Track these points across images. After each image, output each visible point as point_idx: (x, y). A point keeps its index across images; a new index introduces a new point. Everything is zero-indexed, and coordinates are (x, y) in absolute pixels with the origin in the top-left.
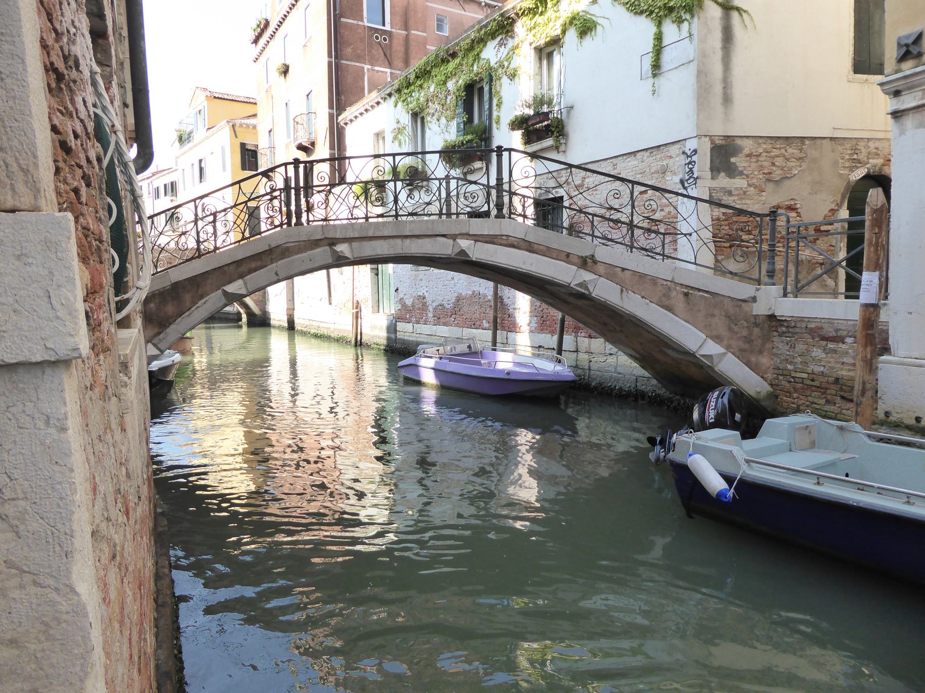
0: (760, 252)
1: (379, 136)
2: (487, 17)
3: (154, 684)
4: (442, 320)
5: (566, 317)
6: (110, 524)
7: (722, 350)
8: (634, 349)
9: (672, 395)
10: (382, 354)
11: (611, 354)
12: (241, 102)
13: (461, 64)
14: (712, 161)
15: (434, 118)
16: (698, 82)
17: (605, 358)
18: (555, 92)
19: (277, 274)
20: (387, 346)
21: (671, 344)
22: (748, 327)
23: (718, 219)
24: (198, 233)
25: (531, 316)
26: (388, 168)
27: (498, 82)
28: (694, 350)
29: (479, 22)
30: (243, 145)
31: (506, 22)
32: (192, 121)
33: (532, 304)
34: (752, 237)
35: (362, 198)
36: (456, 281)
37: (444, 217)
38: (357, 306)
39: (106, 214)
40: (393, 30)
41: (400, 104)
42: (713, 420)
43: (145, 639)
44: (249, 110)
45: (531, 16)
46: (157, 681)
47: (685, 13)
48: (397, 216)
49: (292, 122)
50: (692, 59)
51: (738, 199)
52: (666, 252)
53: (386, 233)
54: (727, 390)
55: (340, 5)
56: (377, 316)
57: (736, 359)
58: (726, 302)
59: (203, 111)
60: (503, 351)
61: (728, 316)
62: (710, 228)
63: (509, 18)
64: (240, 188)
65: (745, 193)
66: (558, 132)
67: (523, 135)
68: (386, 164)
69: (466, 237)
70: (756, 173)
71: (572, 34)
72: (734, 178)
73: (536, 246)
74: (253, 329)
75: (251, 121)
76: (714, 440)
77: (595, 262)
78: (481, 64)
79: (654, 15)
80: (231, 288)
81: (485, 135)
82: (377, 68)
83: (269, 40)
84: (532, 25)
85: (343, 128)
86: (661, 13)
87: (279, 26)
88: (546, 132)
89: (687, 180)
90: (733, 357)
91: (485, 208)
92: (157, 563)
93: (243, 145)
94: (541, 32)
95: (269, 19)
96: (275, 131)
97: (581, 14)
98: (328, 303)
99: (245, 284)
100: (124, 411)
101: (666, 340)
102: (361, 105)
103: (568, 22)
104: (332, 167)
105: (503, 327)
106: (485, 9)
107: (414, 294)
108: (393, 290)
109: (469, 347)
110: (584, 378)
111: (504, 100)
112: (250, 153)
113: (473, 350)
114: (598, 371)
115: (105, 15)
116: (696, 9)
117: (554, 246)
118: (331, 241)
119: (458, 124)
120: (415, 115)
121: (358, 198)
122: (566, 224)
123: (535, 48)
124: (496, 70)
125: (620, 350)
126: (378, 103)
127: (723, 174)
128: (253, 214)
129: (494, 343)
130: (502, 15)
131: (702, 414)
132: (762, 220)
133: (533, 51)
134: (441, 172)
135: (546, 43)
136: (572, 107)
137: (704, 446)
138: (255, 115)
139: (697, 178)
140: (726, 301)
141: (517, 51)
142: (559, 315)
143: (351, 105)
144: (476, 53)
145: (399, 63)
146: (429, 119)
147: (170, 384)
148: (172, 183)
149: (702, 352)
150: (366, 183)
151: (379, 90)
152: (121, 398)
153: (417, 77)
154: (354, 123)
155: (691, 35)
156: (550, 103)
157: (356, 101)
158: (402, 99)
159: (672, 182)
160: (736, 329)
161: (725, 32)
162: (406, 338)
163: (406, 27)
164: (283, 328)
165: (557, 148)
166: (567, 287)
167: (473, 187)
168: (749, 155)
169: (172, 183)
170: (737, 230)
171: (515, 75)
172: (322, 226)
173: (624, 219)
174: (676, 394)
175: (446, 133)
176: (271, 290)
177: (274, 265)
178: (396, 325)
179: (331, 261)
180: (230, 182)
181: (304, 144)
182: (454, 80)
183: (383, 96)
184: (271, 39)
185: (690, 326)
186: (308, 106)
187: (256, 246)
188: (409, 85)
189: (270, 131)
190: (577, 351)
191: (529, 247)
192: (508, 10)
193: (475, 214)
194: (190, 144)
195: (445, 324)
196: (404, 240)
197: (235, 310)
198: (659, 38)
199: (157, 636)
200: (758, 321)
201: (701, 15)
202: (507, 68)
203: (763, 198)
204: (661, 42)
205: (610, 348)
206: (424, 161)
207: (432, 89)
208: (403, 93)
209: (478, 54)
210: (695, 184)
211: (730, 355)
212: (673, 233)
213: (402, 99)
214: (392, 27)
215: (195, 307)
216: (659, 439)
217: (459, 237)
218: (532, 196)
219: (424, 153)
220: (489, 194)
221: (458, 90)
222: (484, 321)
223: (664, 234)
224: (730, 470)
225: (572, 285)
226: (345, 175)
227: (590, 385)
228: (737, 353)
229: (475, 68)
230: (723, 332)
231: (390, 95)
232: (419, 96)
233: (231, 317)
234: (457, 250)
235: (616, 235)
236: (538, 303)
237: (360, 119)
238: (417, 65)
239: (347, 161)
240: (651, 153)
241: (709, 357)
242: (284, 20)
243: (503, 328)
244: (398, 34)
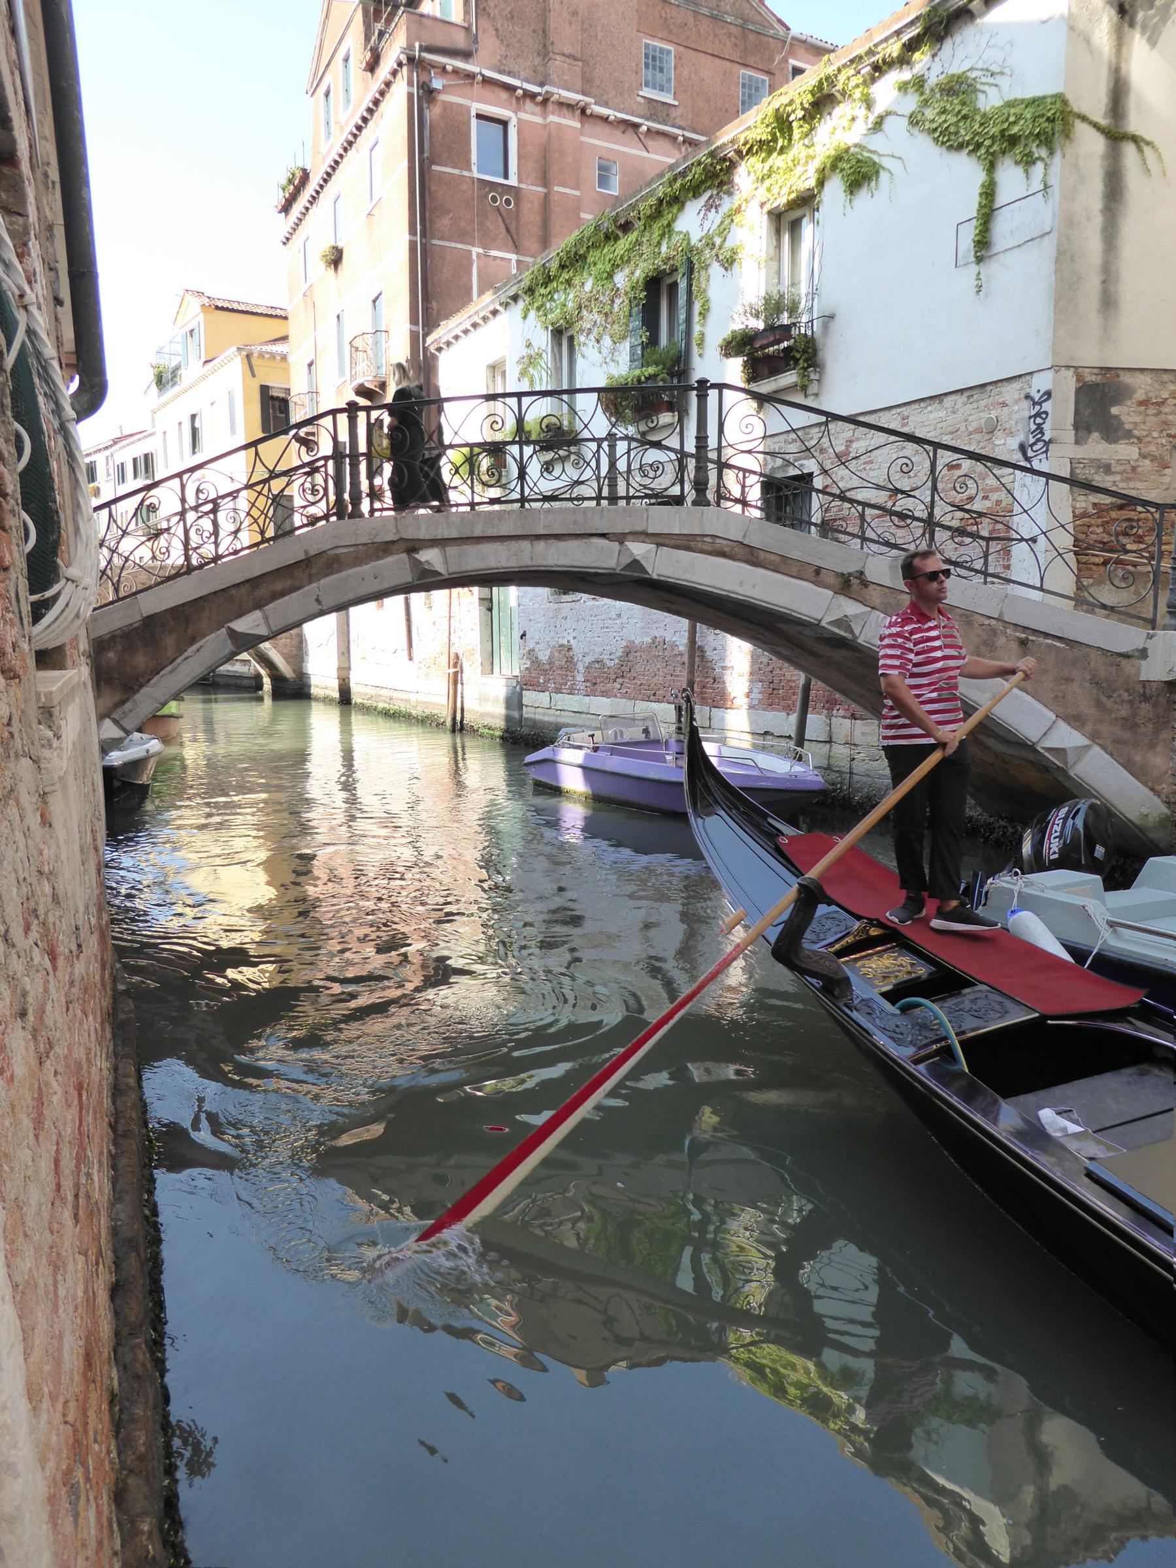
0: (1156, 572)
1: (496, 369)
2: (685, 158)
4: (600, 687)
7: (1084, 741)
9: (992, 819)
10: (498, 747)
13: (638, 243)
14: (1077, 412)
15: (592, 337)
16: (1057, 271)
18: (804, 289)
19: (318, 601)
20: (506, 731)
21: (993, 728)
22: (1130, 702)
23: (1084, 515)
25: (751, 681)
27: (703, 273)
28: (1034, 740)
29: (672, 167)
30: (264, 389)
31: (718, 167)
32: (179, 348)
33: (754, 659)
34: (1142, 546)
35: (464, 470)
36: (624, 620)
37: (604, 503)
38: (456, 662)
39: (13, 450)
40: (522, 186)
41: (532, 314)
42: (1056, 856)
43: (89, 1175)
44: (274, 328)
45: (763, 155)
47: (1038, 146)
48: (523, 500)
49: (347, 348)
50: (1048, 230)
51: (1122, 481)
52: (991, 570)
53: (504, 531)
54: (1083, 805)
55: (431, 142)
56: (489, 679)
57: (1108, 757)
58: (1092, 656)
59: (196, 331)
61: (1095, 682)
62: (1070, 527)
63: (724, 159)
64: (257, 454)
65: (1134, 469)
66: (806, 360)
68: (506, 411)
69: (642, 538)
70: (1155, 434)
71: (835, 187)
72: (1115, 441)
73: (762, 555)
74: (282, 703)
76: (1056, 888)
77: (865, 584)
78: (674, 241)
79: (983, 151)
80: (242, 625)
81: (679, 365)
82: (493, 253)
83: (308, 205)
84: (765, 171)
85: (434, 357)
86: (995, 147)
88: (786, 360)
89: (1032, 446)
90: (1103, 752)
91: (676, 491)
92: (116, 1069)
93: (264, 389)
95: (308, 167)
96: (320, 365)
97: (852, 150)
98: (407, 657)
99: (266, 618)
100: (47, 790)
103: (828, 165)
105: (703, 698)
106: (683, 149)
107: (553, 643)
108: (517, 634)
109: (646, 731)
111: (714, 305)
112: (277, 404)
113: (652, 736)
117: (795, 554)
118: (409, 545)
121: (457, 472)
123: (770, 213)
124: (700, 252)
126: (495, 313)
127: (1095, 435)
128: (281, 502)
130: (712, 154)
132: (1162, 516)
133: (765, 217)
136: (832, 317)
138: (284, 338)
139: (1050, 441)
140: (1093, 655)
141: (737, 218)
142: (800, 678)
143: (447, 317)
144: (666, 223)
145: (531, 243)
146: (582, 339)
147: (144, 790)
148: (146, 456)
149: (1048, 743)
150: (471, 446)
151: (497, 290)
152: (42, 766)
153: (562, 267)
154: (453, 348)
156: (793, 309)
157: (458, 311)
158: (536, 305)
159: (1006, 447)
160: (1109, 704)
161: (1110, 180)
162: (538, 717)
163: (545, 180)
165: (804, 388)
166: (814, 626)
167: (653, 455)
168: (1144, 403)
170: (1117, 534)
173: (920, 512)
174: (1000, 817)
175: (612, 364)
176: (309, 628)
177: (314, 585)
178: (521, 695)
179: (409, 579)
181: (366, 385)
182: (627, 271)
183: (503, 299)
186: (376, 319)
187: (287, 553)
188: (548, 280)
189: (310, 365)
190: (830, 741)
191: (751, 556)
192: (724, 145)
194: (176, 389)
195: (605, 694)
196: (535, 543)
197: (252, 671)
198: (989, 192)
199: (114, 1182)
200: (1148, 692)
202: (720, 248)
203: (1166, 480)
204: (992, 201)
206: (573, 411)
207: (588, 287)
208: (537, 294)
209: (669, 225)
210: (1046, 452)
211: (1096, 749)
212: (1005, 539)
213: (536, 305)
214: (520, 181)
215: (182, 658)
217: (630, 537)
218: (758, 469)
219: (572, 392)
220: (682, 468)
221: (633, 288)
224: (1081, 939)
225: (823, 623)
228: (1110, 748)
229: (664, 248)
230: (1086, 707)
231: (515, 298)
232: (566, 299)
233: (246, 682)
234: (626, 561)
236: (766, 656)
237: (464, 341)
238: (563, 245)
240: (969, 397)
241: (1060, 752)
243: (704, 701)
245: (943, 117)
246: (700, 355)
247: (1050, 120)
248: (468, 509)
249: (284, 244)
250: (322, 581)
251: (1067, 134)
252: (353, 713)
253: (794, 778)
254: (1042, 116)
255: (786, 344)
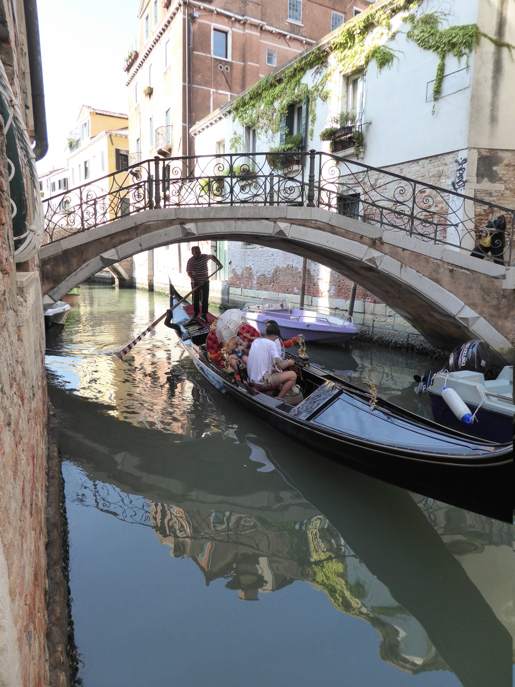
1: (220, 144)
2: (307, 50)
3: (45, 530)
4: (263, 286)
5: (358, 286)
6: (5, 396)
7: (477, 315)
8: (408, 312)
9: (434, 349)
11: (390, 316)
12: (117, 117)
13: (285, 88)
14: (478, 169)
15: (263, 130)
17: (386, 319)
18: (358, 110)
19: (140, 245)
20: (222, 305)
21: (437, 308)
22: (497, 298)
23: (480, 215)
24: (82, 213)
25: (330, 285)
26: (227, 168)
27: (313, 102)
28: (455, 314)
29: (300, 54)
30: (117, 151)
31: (321, 55)
32: (79, 131)
33: (332, 275)
35: (206, 188)
36: (275, 257)
37: (268, 204)
39: (7, 171)
40: (234, 62)
41: (237, 119)
42: (464, 365)
43: (37, 495)
45: (342, 49)
46: (47, 528)
47: (465, 48)
48: (232, 202)
49: (154, 133)
50: (468, 86)
54: (477, 343)
55: (193, 41)
58: (482, 277)
59: (87, 124)
60: (308, 310)
61: (483, 289)
63: (324, 51)
64: (114, 179)
65: (502, 195)
66: (358, 143)
67: (331, 144)
69: (284, 220)
71: (373, 65)
72: (495, 182)
75: (124, 132)
76: (463, 378)
77: (382, 243)
78: (301, 88)
79: (440, 50)
80: (108, 255)
81: (302, 144)
82: (220, 92)
84: (342, 57)
85: (193, 138)
87: (146, 57)
88: (350, 143)
90: (484, 320)
91: (300, 200)
92: (49, 449)
93: (117, 151)
94: (349, 62)
95: (138, 51)
96: (142, 140)
97: (381, 48)
99: (117, 252)
100: (20, 324)
101: (433, 305)
102: (207, 120)
103: (370, 55)
104: (184, 163)
105: (309, 292)
106: (305, 46)
110: (368, 334)
111: (318, 117)
112: (123, 157)
113: (285, 308)
114: (380, 328)
115: (6, 22)
116: (474, 45)
118: (181, 221)
119: (281, 135)
120: (248, 128)
121: (203, 189)
122: (361, 213)
123: (344, 76)
125: (397, 312)
126: (220, 118)
127: (486, 179)
128: (124, 201)
129: (302, 304)
130: (319, 49)
131: (456, 360)
134: (267, 170)
135: (352, 71)
136: (370, 124)
137: (456, 382)
138: (127, 128)
139: (466, 181)
140: (482, 277)
141: (329, 78)
142: (352, 284)
143: (199, 120)
144: (297, 79)
145: (237, 87)
146: (259, 131)
147: (62, 326)
148: (65, 179)
149: (461, 315)
150: (209, 178)
151: (221, 108)
152: (18, 314)
153: (251, 98)
154: (201, 134)
155: (468, 67)
156: (353, 120)
157: (204, 117)
158: (239, 115)
159: (446, 183)
160: (488, 299)
162: (236, 299)
163: (244, 60)
164: (145, 289)
166: (360, 261)
167: (290, 184)
168: (508, 165)
169: (65, 179)
171: (327, 97)
172: (175, 209)
173: (408, 211)
178: (229, 289)
180: (108, 174)
181: (163, 150)
182: (279, 101)
183: (224, 113)
184: (139, 67)
185: (453, 295)
186: (167, 120)
187: (127, 224)
188: (244, 104)
189: (138, 140)
190: (364, 313)
191: (332, 229)
192: (324, 45)
193: (293, 203)
194: (78, 150)
195: (266, 290)
196: (237, 221)
197: (110, 276)
198: (442, 69)
199: (48, 498)
200: (505, 294)
201: (479, 50)
202: (321, 91)
204: (443, 73)
205: (390, 311)
206: (254, 161)
207: (262, 108)
208: (239, 110)
209: (299, 81)
210: (464, 186)
211: (482, 318)
213: (239, 115)
214: (232, 59)
215: (80, 269)
216: (422, 377)
217: (279, 220)
218: (336, 191)
221: (282, 109)
222: (295, 288)
223: (437, 225)
224: (473, 401)
225: (363, 260)
226: (194, 170)
227: (372, 339)
228: (488, 318)
229: (296, 91)
231: (230, 112)
232: (252, 113)
233: (107, 281)
234: (277, 230)
235: (399, 222)
236: (337, 274)
237: (206, 130)
238: (251, 89)
239: (196, 159)
240: (430, 161)
241: (466, 319)
242: (150, 52)
243: (309, 294)
244: (237, 65)
245: (422, 34)
246: (311, 140)
247: (471, 36)
248: (207, 205)
249: (127, 85)
250: (142, 236)
251: (478, 43)
252: (155, 296)
253: (344, 327)
254: (467, 34)
255: (349, 135)
